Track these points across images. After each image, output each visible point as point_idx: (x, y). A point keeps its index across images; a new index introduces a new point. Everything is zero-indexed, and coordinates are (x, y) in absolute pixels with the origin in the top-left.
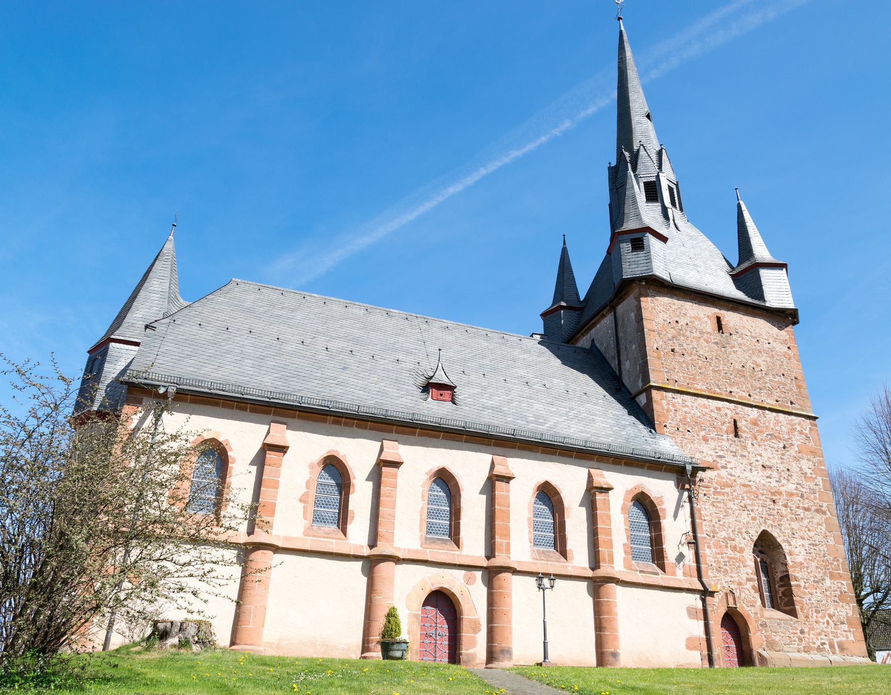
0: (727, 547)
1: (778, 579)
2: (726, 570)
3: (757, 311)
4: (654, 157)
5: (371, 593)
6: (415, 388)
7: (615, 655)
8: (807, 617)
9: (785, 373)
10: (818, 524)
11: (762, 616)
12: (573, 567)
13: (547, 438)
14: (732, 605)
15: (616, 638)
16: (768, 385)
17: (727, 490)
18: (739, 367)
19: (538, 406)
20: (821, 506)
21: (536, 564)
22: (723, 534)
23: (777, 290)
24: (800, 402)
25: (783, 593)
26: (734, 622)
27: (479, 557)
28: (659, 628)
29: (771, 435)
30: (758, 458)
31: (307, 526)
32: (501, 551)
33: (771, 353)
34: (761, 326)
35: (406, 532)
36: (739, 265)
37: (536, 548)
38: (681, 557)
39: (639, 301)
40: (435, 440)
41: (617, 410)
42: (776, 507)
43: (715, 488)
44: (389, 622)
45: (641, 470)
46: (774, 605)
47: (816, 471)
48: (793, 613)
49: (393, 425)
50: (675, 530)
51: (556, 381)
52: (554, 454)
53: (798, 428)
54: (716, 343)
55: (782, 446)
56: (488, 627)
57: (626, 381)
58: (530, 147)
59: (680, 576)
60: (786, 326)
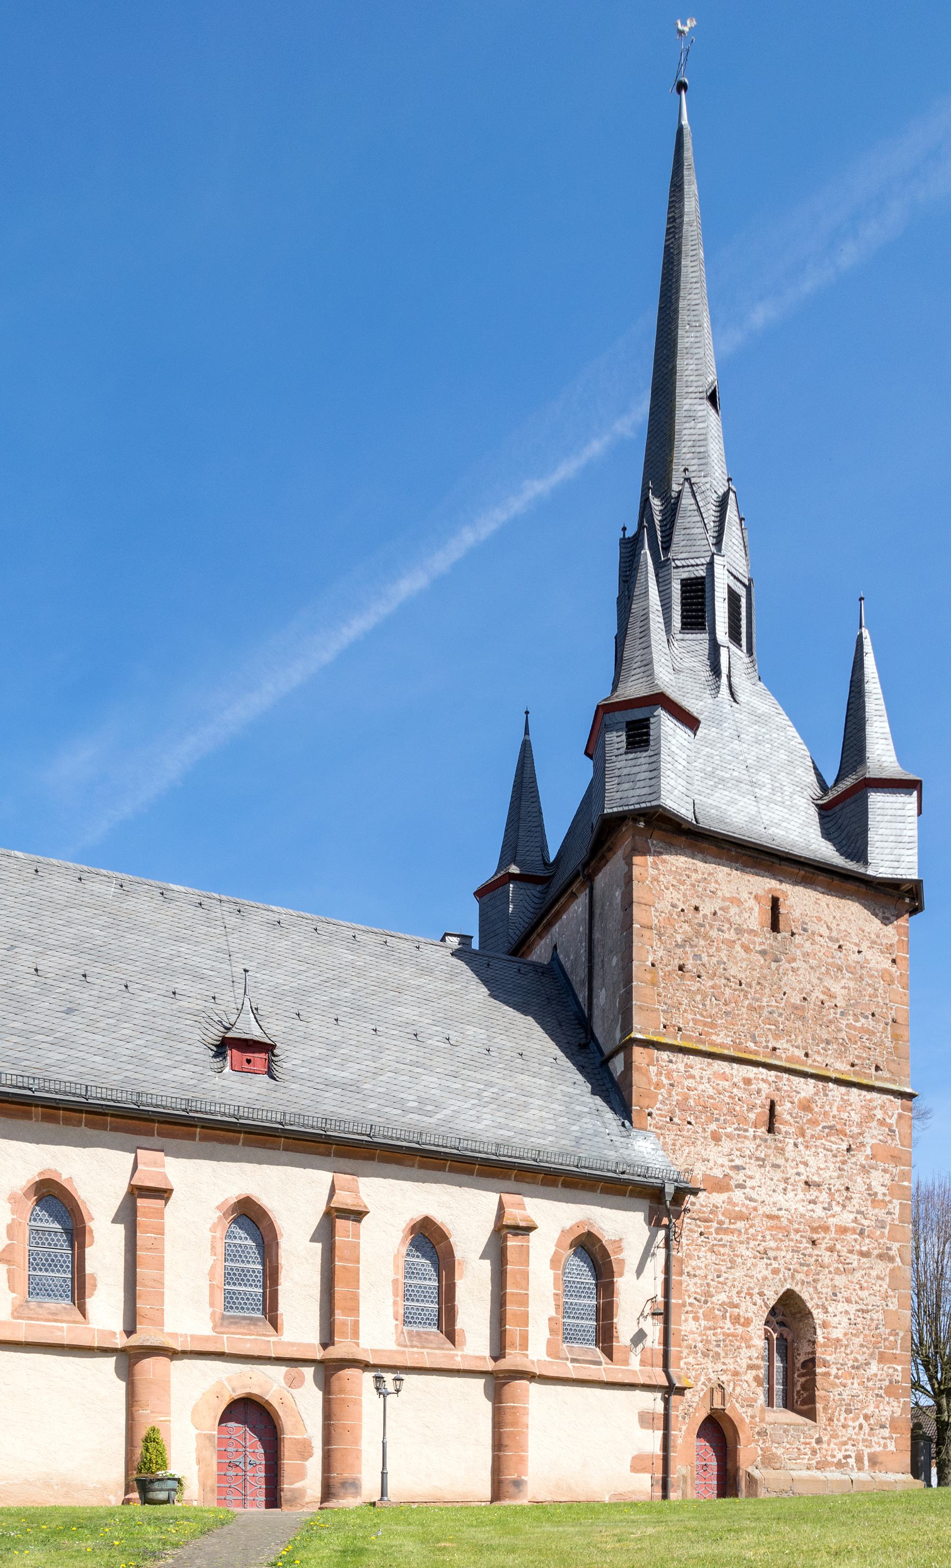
0: (724, 1317)
1: (798, 1365)
2: (718, 1354)
3: (850, 886)
4: (710, 514)
5: (132, 1406)
6: (202, 1048)
7: (518, 1484)
8: (831, 1420)
9: (878, 1011)
10: (878, 1278)
11: (762, 1420)
12: (463, 1357)
13: (430, 1141)
14: (717, 1405)
15: (522, 1460)
16: (843, 1034)
17: (740, 1225)
18: (796, 999)
19: (430, 1080)
20: (889, 1249)
21: (404, 1352)
22: (723, 1297)
23: (894, 840)
24: (893, 1066)
25: (804, 1387)
26: (718, 1431)
27: (310, 1345)
28: (590, 1443)
29: (831, 1128)
30: (802, 1168)
31: (18, 1302)
32: (344, 1335)
33: (858, 971)
34: (850, 916)
35: (187, 1304)
36: (837, 781)
37: (406, 1329)
38: (640, 1336)
39: (630, 865)
40: (230, 1147)
41: (571, 1084)
42: (816, 1252)
43: (721, 1223)
44: (147, 1450)
45: (589, 1195)
46: (788, 1404)
47: (894, 1190)
48: (811, 1414)
49: (153, 1121)
50: (635, 1292)
51: (471, 1030)
52: (441, 1168)
53: (879, 1114)
54: (763, 953)
55: (844, 1146)
56: (323, 1450)
57: (598, 1032)
58: (566, 470)
59: (634, 1366)
60: (898, 917)
